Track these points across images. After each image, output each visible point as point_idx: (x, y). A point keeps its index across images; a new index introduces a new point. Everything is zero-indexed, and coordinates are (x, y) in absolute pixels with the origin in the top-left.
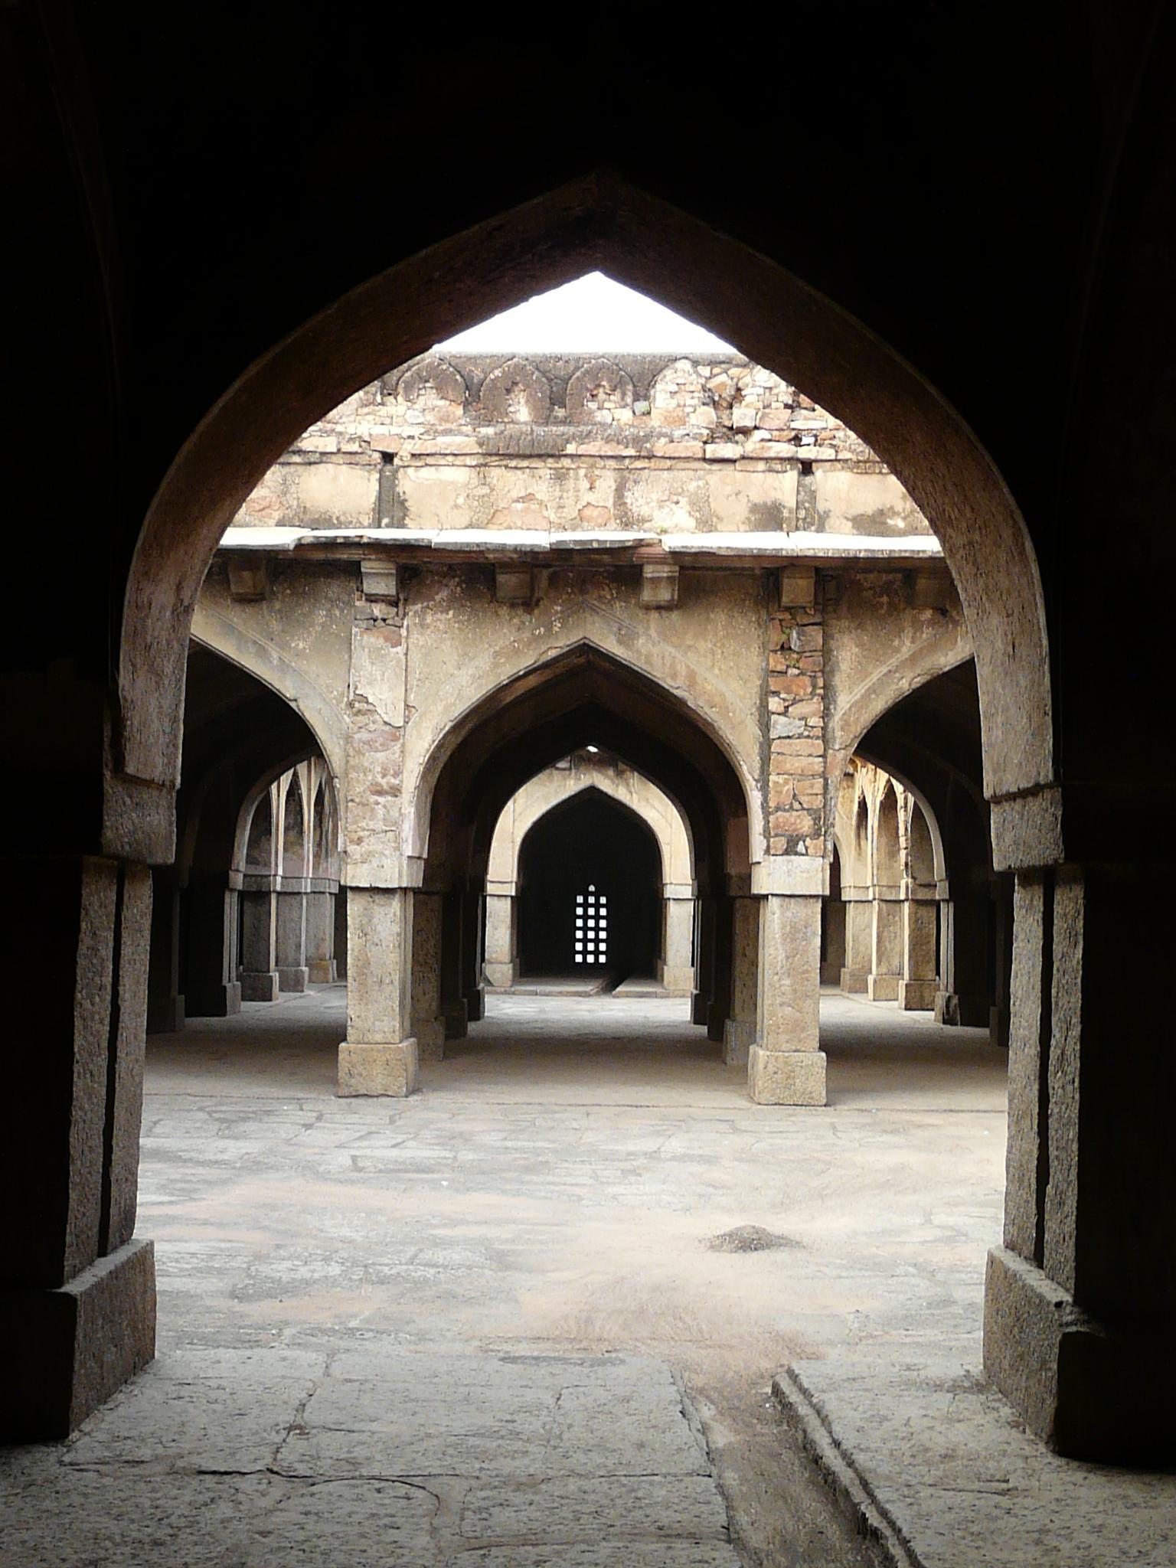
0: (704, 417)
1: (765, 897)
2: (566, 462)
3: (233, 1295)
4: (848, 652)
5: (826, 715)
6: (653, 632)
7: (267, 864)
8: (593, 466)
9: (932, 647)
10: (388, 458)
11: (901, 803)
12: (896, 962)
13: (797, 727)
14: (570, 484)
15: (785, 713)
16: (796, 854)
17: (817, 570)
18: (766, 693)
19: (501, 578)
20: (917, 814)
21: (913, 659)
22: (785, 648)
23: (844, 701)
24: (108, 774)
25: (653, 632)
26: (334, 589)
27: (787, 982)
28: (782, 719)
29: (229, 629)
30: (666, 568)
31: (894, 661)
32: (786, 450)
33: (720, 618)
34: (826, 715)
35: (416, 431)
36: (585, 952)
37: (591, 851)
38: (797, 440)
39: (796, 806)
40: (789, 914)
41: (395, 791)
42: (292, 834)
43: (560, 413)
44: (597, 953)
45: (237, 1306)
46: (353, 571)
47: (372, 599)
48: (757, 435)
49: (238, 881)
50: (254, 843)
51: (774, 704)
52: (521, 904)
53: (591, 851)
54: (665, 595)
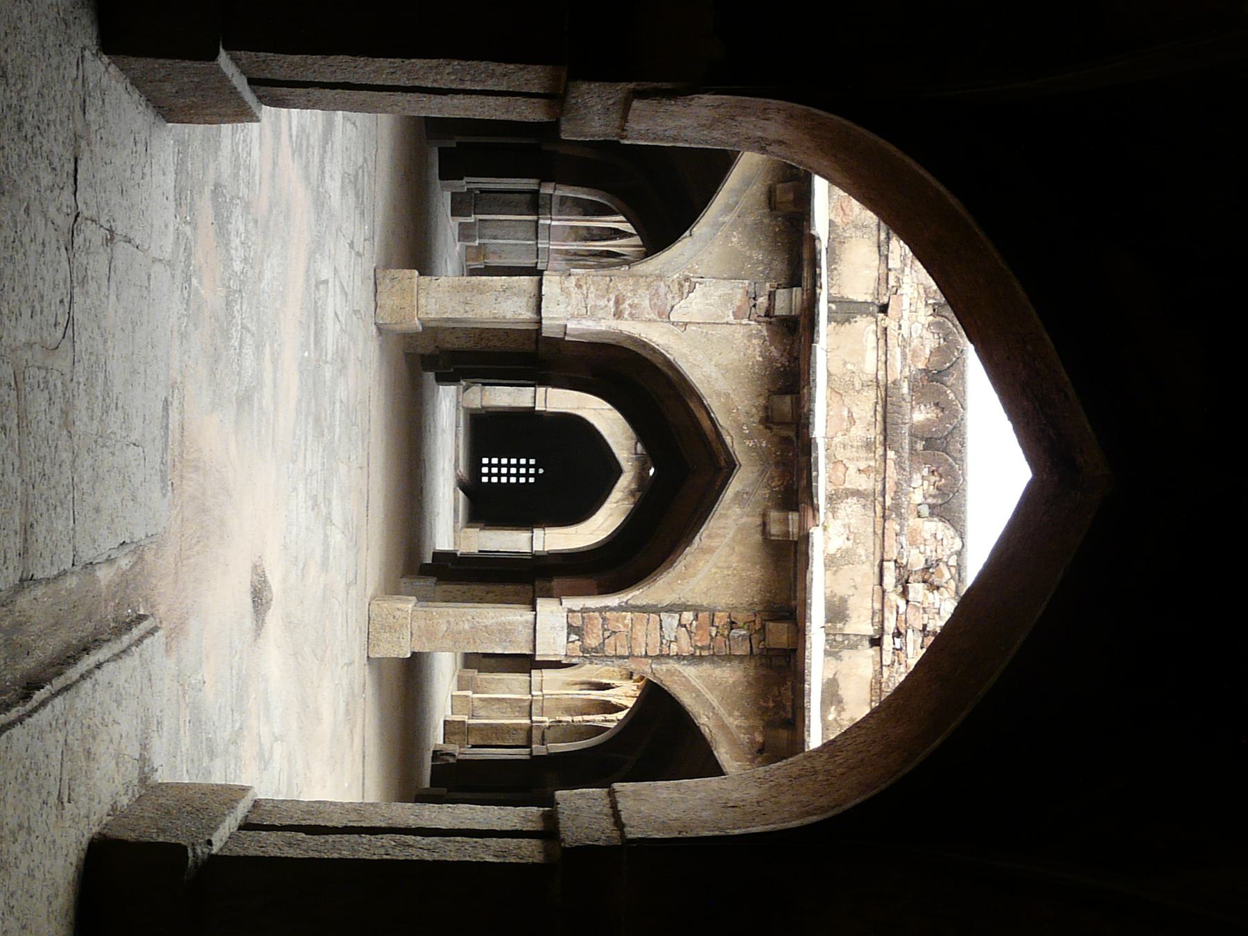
0: (916, 560)
1: (534, 609)
2: (880, 451)
3: (217, 186)
4: (729, 675)
5: (679, 657)
6: (745, 519)
7: (560, 213)
8: (877, 472)
9: (733, 742)
10: (884, 309)
11: (609, 717)
12: (482, 713)
13: (669, 634)
14: (863, 454)
15: (681, 625)
16: (569, 634)
17: (795, 650)
18: (696, 610)
19: (788, 399)
20: (600, 730)
21: (723, 727)
22: (732, 624)
23: (690, 672)
24: (632, 86)
25: (745, 519)
26: (779, 265)
27: (467, 626)
28: (676, 623)
29: (747, 182)
30: (796, 530)
31: (722, 712)
32: (890, 626)
33: (756, 573)
34: (679, 657)
35: (905, 331)
36: (490, 465)
37: (573, 472)
38: (898, 634)
39: (607, 634)
40: (521, 628)
41: (618, 315)
42: (585, 233)
43: (920, 446)
44: (490, 475)
45: (208, 189)
46: (793, 281)
47: (771, 296)
48: (902, 603)
49: (547, 189)
50: (577, 202)
51: (688, 616)
52: (529, 414)
53: (573, 472)
54: (775, 529)
